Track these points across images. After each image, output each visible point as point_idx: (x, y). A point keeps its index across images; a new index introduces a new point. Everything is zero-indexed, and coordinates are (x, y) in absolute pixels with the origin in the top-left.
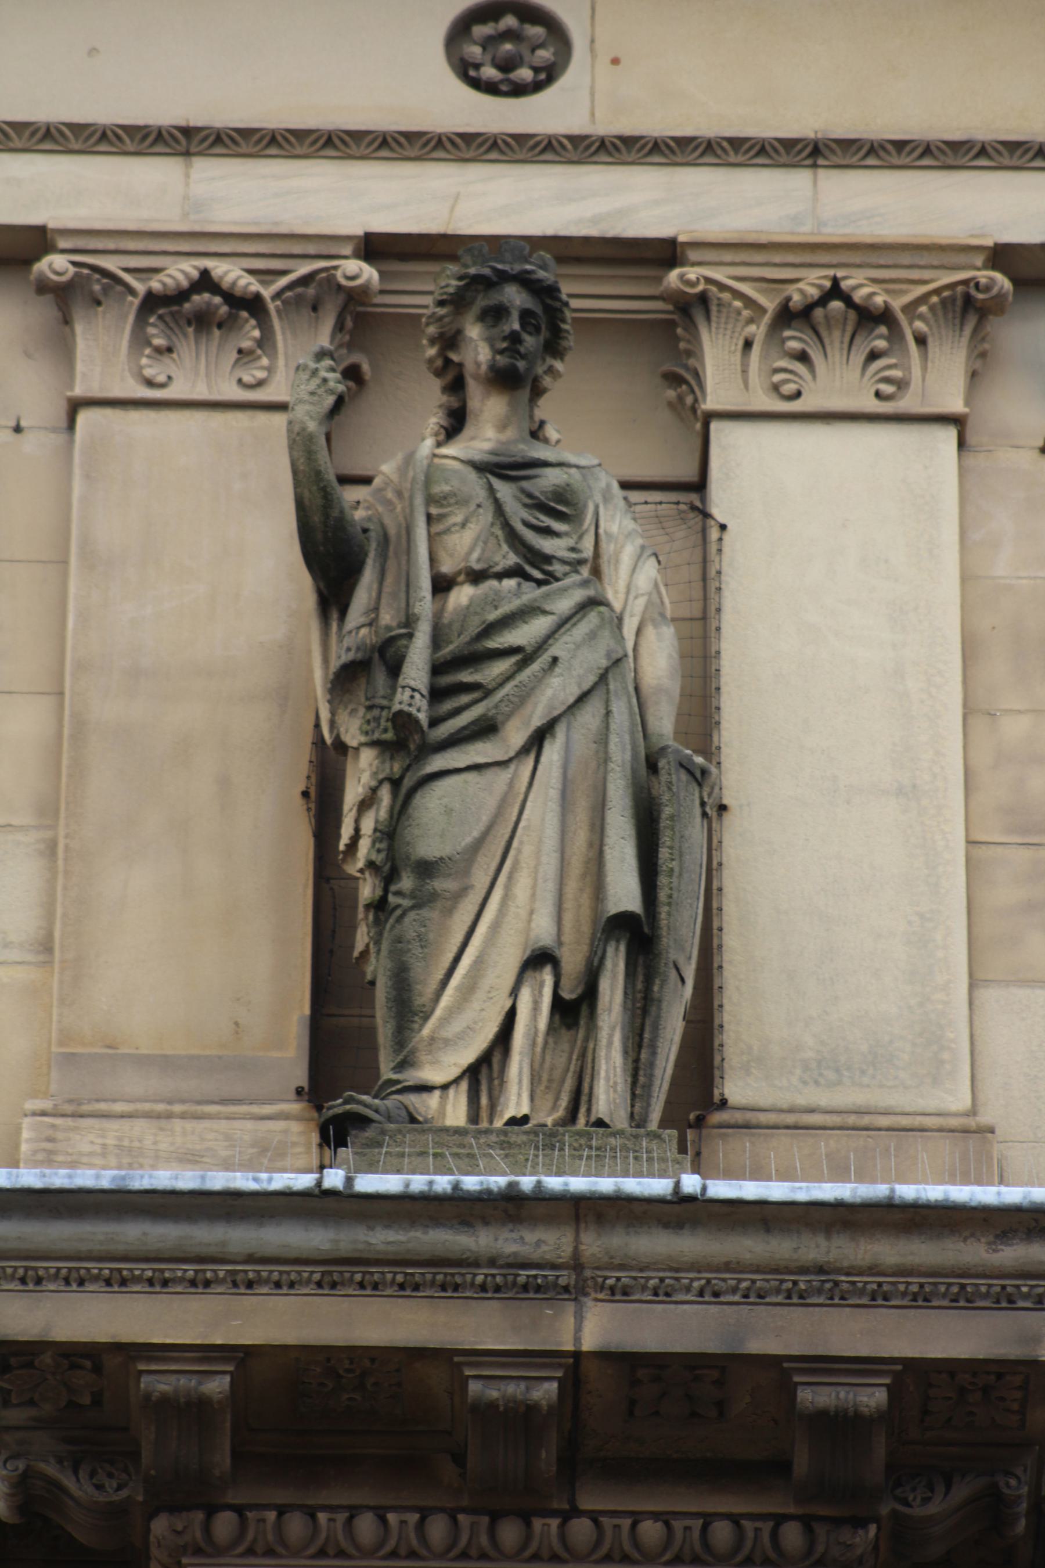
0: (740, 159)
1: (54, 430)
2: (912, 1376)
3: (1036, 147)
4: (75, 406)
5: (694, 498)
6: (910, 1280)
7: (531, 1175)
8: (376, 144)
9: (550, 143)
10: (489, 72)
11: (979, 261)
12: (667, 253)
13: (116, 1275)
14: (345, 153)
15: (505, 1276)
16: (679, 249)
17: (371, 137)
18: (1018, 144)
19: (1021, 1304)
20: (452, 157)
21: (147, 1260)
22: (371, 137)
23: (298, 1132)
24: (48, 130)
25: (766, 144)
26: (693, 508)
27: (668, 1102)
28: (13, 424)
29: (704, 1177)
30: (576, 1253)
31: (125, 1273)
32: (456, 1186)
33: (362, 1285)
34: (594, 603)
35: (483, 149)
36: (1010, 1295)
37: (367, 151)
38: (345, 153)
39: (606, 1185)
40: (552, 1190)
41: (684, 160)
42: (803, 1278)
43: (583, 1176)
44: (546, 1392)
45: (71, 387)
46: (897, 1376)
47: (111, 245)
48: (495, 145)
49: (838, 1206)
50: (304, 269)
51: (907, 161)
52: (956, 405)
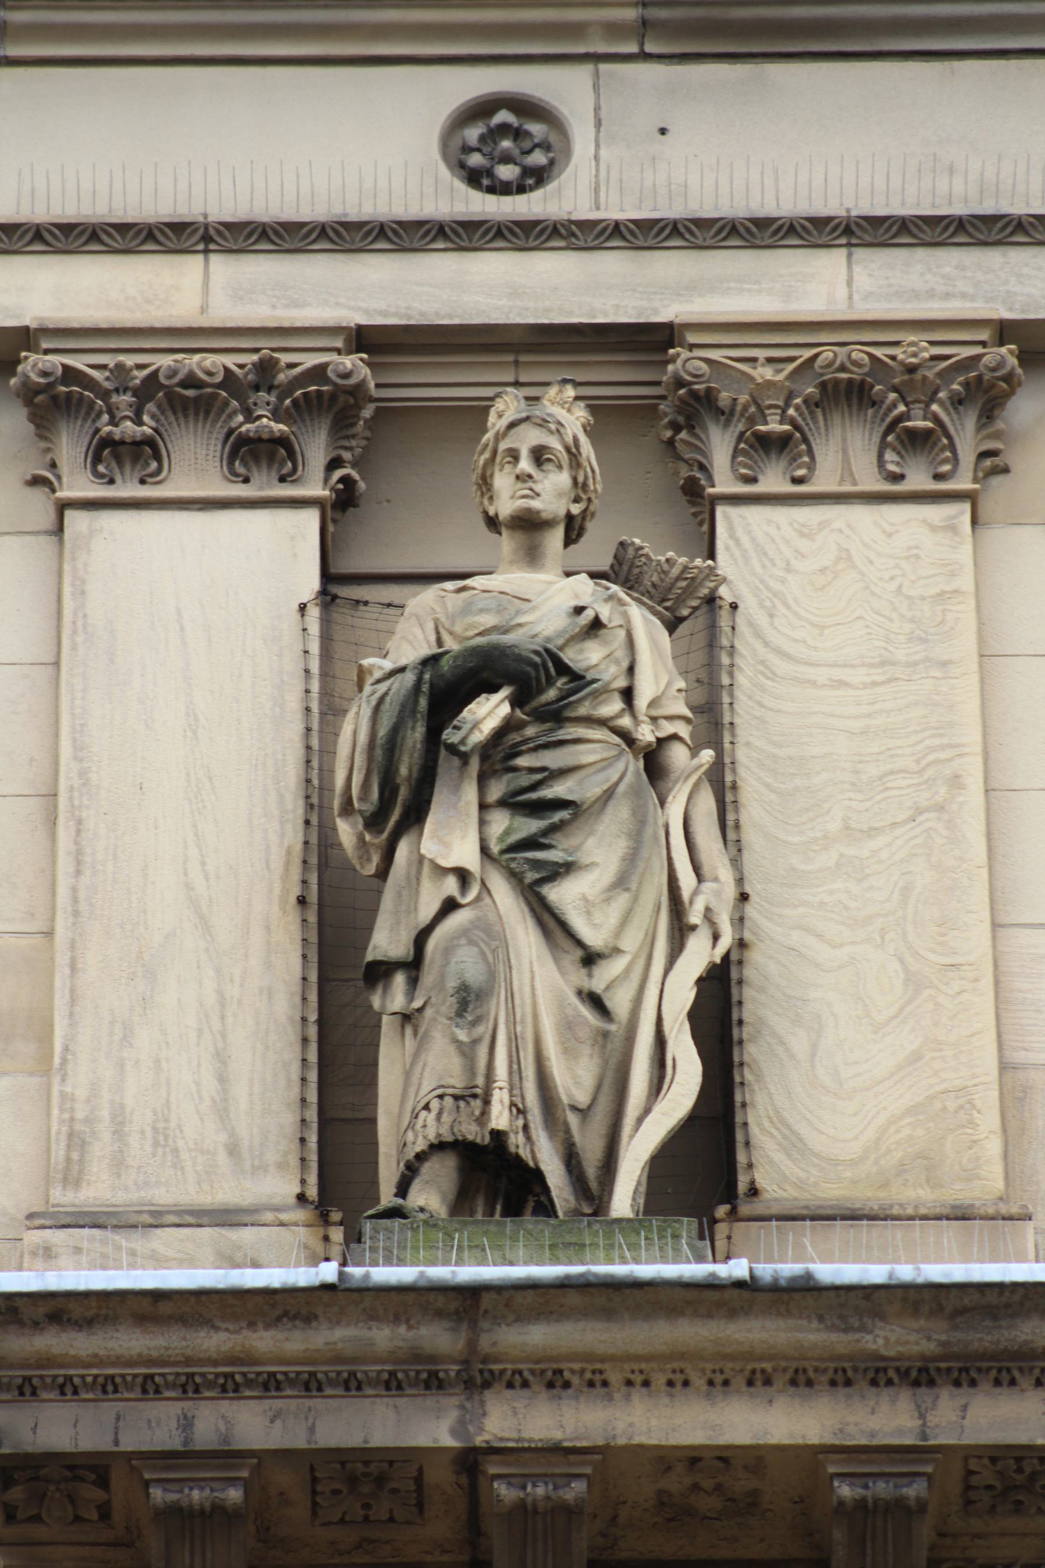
6: (44, 1373)
7: (881, 1261)
8: (491, 235)
9: (555, 228)
12: (653, 340)
15: (405, 1372)
16: (676, 332)
17: (946, 221)
19: (167, 1394)
20: (805, 243)
22: (946, 221)
24: (499, 228)
25: (558, 226)
31: (238, 1377)
35: (428, 239)
37: (189, 243)
42: (412, 1368)
46: (257, 1469)
49: (157, 1296)
50: (311, 360)
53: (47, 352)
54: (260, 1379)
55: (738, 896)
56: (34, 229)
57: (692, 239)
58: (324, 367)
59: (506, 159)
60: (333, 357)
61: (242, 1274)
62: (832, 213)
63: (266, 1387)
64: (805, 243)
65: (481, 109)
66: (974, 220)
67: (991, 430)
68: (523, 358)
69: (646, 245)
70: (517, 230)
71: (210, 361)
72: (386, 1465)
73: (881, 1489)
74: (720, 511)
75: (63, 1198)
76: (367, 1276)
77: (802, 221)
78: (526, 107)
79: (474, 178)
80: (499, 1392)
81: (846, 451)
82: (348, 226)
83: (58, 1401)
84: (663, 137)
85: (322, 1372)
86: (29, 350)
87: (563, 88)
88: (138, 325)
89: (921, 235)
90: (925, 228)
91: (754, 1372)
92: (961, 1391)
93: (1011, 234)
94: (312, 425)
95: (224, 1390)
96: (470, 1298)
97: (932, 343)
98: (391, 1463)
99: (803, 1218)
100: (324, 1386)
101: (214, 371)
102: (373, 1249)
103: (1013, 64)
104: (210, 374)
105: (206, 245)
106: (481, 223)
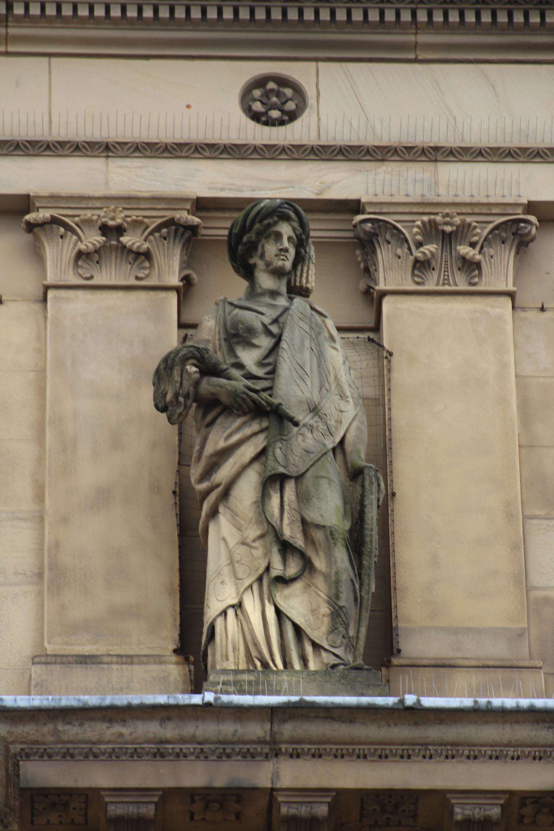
0: (36, 152)
1: (37, 301)
2: (339, 797)
4: (47, 288)
5: (372, 335)
9: (538, 152)
10: (275, 114)
11: (520, 210)
12: (354, 207)
20: (173, 156)
21: (336, 743)
23: (175, 671)
28: (541, 306)
29: (419, 695)
32: (489, 703)
33: (468, 757)
34: (271, 388)
39: (365, 700)
41: (355, 158)
43: (283, 695)
44: (322, 810)
45: (45, 279)
46: (335, 798)
47: (392, 210)
48: (48, 147)
51: (470, 159)
52: (511, 287)
62: (500, 146)
65: (260, 82)
70: (118, 146)
74: (387, 305)
76: (489, 703)
77: (24, 142)
78: (283, 82)
79: (256, 117)
80: (484, 762)
83: (129, 760)
84: (349, 98)
87: (298, 71)
92: (338, 760)
93: (251, 154)
106: (186, 144)
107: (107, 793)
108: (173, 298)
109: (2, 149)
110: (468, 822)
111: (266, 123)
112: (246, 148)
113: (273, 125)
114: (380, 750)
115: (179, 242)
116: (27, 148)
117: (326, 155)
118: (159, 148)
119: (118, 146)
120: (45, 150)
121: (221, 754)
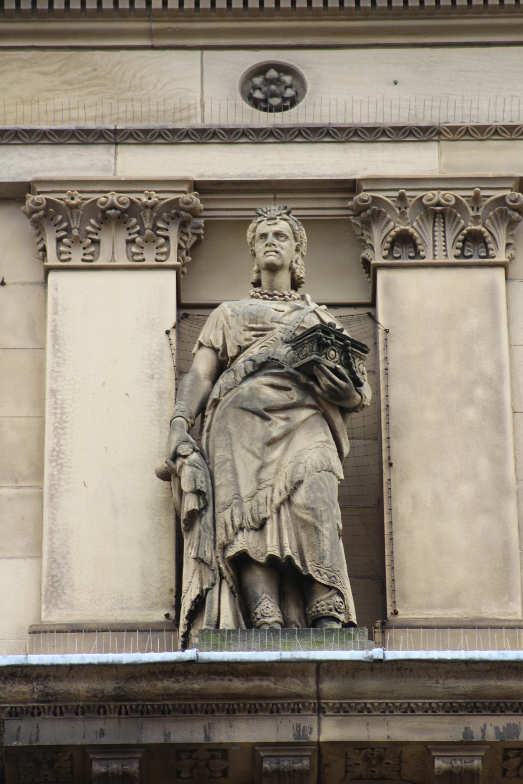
3: (129, 133)
10: (276, 101)
12: (350, 187)
13: (188, 708)
14: (108, 141)
18: (401, 128)
20: (50, 142)
24: (187, 132)
25: (413, 129)
26: (369, 314)
27: (357, 613)
30: (318, 692)
36: (369, 708)
38: (108, 141)
40: (205, 660)
48: (496, 132)
49: (72, 667)
50: (499, 194)
53: (39, 193)
54: (359, 707)
55: (388, 465)
56: (72, 132)
57: (81, 139)
58: (503, 198)
59: (274, 95)
60: (508, 192)
61: (309, 654)
63: (163, 713)
64: (50, 142)
65: (261, 70)
66: (80, 132)
67: (511, 233)
68: (278, 196)
69: (230, 141)
70: (140, 134)
71: (449, 194)
72: (382, 750)
73: (115, 766)
75: (56, 616)
79: (255, 103)
81: (440, 245)
82: (282, 130)
84: (345, 82)
85: (369, 703)
86: (30, 193)
88: (400, 177)
89: (81, 139)
90: (339, 134)
91: (55, 708)
94: (499, 228)
95: (142, 713)
96: (322, 668)
97: (80, 192)
98: (385, 749)
99: (459, 627)
100: (280, 711)
101: (125, 202)
102: (356, 642)
103: (168, 52)
104: (124, 204)
105: (439, 137)
107: (261, 748)
108: (172, 276)
109: (2, 138)
110: (449, 773)
111: (265, 110)
112: (236, 131)
113: (271, 111)
114: (206, 705)
115: (428, 221)
116: (308, 135)
117: (398, 137)
118: (209, 134)
119: (25, 134)
120: (494, 134)
121: (406, 708)
